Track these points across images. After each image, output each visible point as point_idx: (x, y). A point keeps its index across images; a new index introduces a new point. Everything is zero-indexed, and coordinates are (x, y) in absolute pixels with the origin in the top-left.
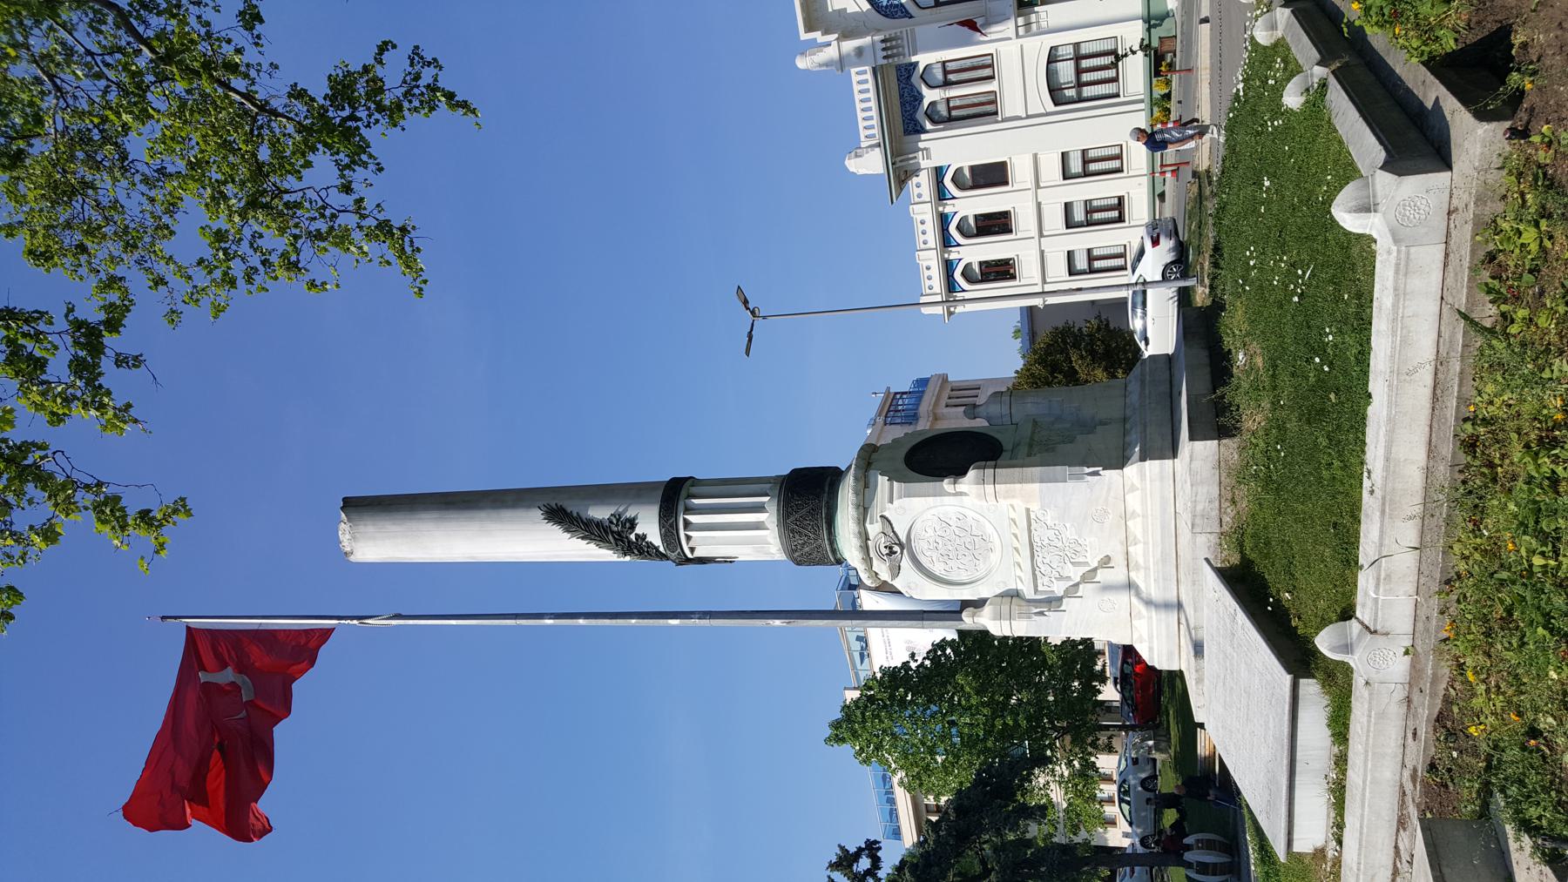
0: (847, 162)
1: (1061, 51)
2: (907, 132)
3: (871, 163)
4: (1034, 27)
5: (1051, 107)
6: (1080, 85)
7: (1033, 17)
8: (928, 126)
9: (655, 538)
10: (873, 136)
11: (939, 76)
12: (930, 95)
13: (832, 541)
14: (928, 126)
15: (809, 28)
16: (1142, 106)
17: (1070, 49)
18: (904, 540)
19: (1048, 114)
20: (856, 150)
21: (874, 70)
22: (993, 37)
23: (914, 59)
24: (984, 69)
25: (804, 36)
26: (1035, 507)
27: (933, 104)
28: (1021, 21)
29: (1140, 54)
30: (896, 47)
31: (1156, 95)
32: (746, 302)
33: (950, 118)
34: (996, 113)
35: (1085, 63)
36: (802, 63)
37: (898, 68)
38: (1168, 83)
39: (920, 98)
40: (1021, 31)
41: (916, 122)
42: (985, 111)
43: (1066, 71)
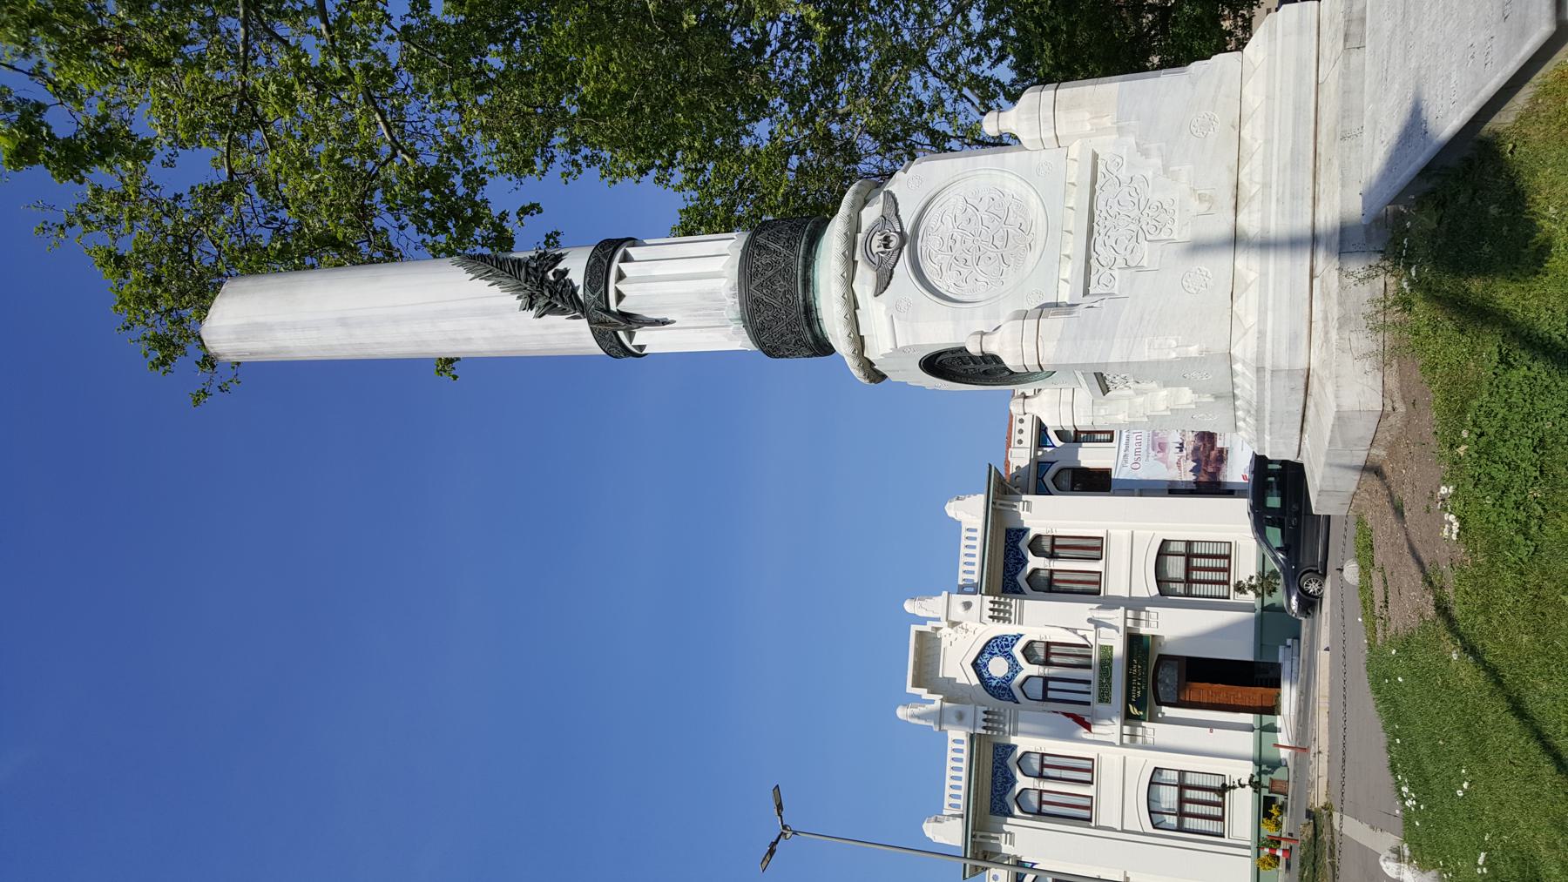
0: (925, 826)
1: (1173, 548)
2: (993, 811)
3: (948, 832)
4: (1140, 739)
5: (1149, 828)
6: (1188, 581)
7: (1139, 731)
8: (1017, 812)
9: (577, 277)
10: (958, 806)
11: (1041, 654)
12: (1022, 782)
13: (809, 263)
14: (1017, 812)
15: (917, 683)
16: (1248, 852)
17: (1174, 776)
18: (908, 230)
19: (1144, 834)
20: (936, 814)
21: (972, 737)
22: (1097, 738)
23: (1014, 740)
24: (1086, 771)
25: (910, 689)
26: (1107, 146)
27: (1035, 571)
28: (1126, 729)
29: (1249, 789)
30: (1005, 612)
31: (1263, 835)
32: (780, 807)
33: (1048, 587)
34: (1090, 820)
35: (1196, 562)
36: (902, 713)
37: (996, 747)
38: (1278, 825)
39: (1013, 781)
40: (1126, 739)
41: (1016, 584)
42: (1080, 815)
43: (1169, 797)
